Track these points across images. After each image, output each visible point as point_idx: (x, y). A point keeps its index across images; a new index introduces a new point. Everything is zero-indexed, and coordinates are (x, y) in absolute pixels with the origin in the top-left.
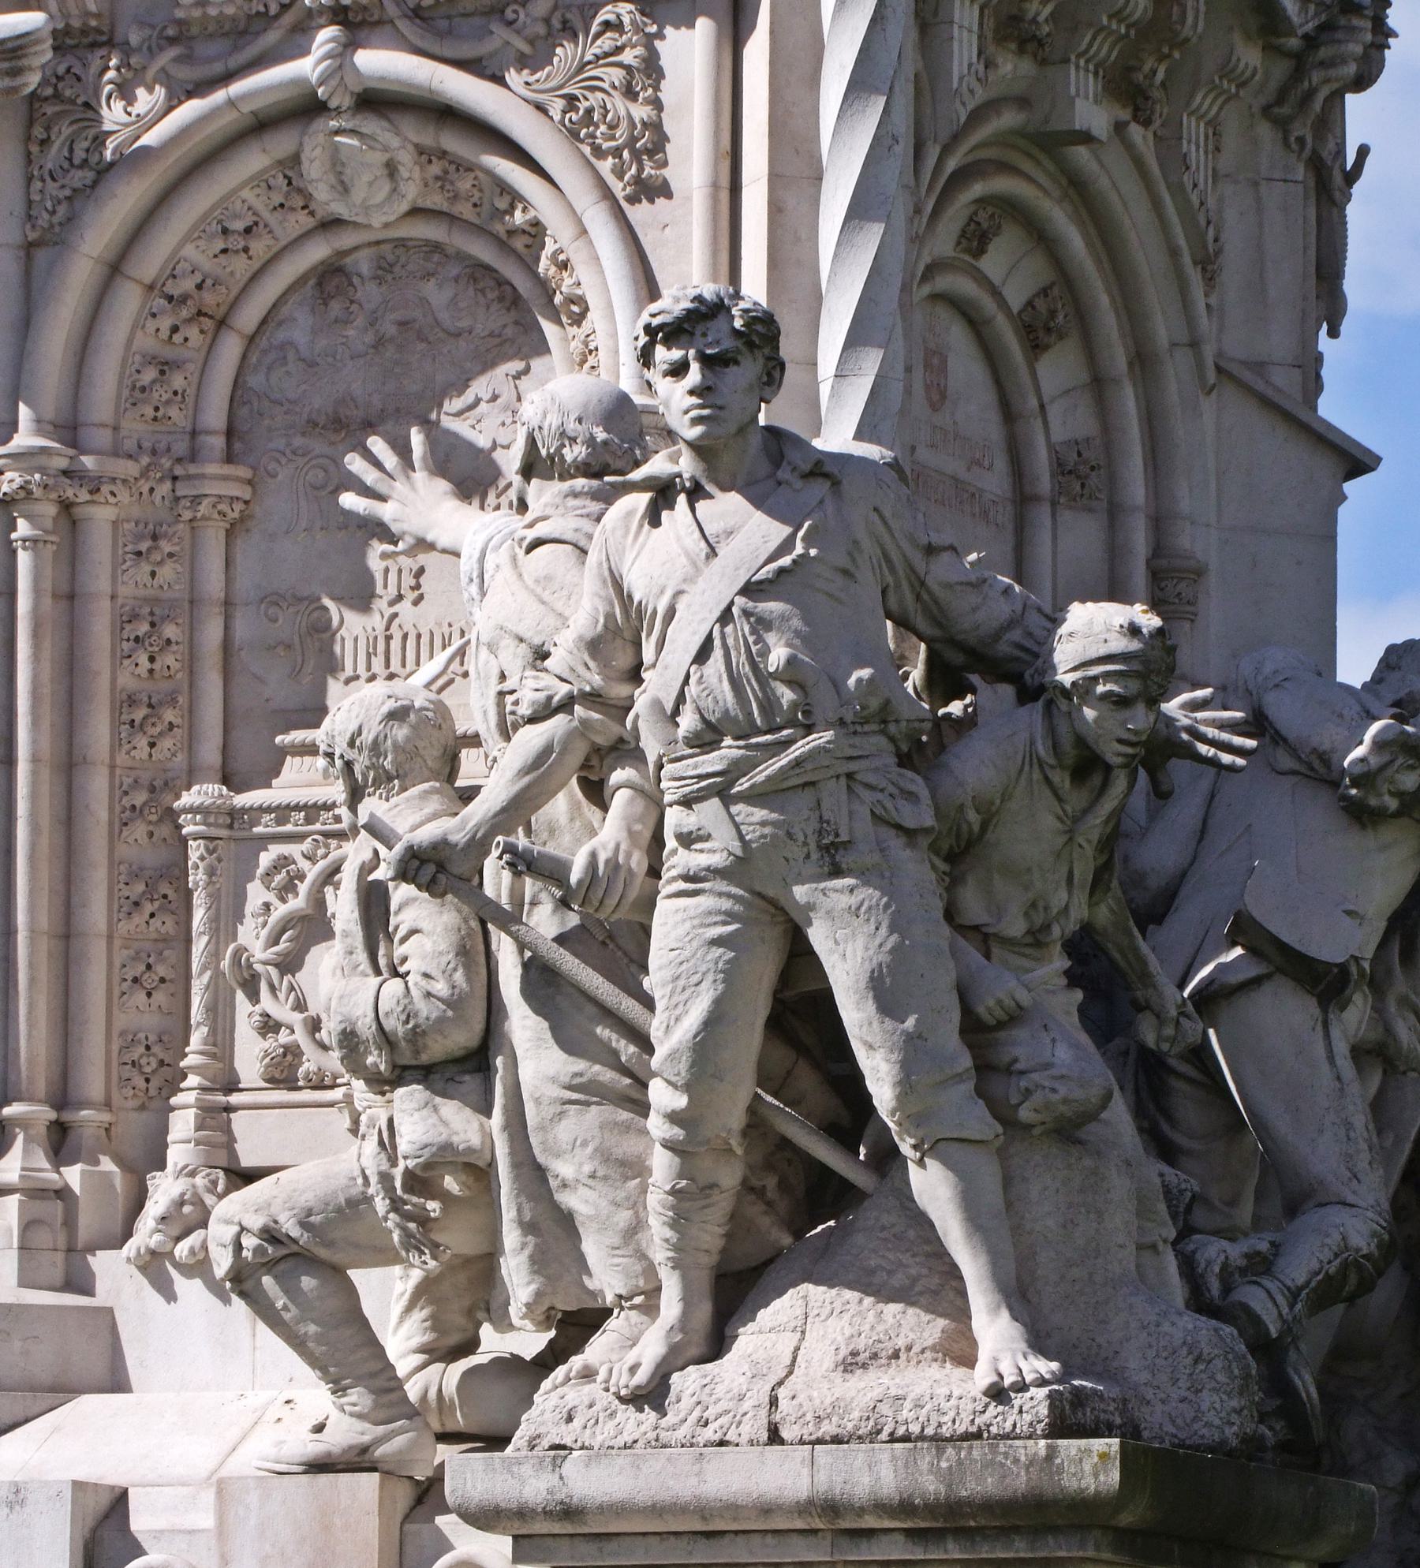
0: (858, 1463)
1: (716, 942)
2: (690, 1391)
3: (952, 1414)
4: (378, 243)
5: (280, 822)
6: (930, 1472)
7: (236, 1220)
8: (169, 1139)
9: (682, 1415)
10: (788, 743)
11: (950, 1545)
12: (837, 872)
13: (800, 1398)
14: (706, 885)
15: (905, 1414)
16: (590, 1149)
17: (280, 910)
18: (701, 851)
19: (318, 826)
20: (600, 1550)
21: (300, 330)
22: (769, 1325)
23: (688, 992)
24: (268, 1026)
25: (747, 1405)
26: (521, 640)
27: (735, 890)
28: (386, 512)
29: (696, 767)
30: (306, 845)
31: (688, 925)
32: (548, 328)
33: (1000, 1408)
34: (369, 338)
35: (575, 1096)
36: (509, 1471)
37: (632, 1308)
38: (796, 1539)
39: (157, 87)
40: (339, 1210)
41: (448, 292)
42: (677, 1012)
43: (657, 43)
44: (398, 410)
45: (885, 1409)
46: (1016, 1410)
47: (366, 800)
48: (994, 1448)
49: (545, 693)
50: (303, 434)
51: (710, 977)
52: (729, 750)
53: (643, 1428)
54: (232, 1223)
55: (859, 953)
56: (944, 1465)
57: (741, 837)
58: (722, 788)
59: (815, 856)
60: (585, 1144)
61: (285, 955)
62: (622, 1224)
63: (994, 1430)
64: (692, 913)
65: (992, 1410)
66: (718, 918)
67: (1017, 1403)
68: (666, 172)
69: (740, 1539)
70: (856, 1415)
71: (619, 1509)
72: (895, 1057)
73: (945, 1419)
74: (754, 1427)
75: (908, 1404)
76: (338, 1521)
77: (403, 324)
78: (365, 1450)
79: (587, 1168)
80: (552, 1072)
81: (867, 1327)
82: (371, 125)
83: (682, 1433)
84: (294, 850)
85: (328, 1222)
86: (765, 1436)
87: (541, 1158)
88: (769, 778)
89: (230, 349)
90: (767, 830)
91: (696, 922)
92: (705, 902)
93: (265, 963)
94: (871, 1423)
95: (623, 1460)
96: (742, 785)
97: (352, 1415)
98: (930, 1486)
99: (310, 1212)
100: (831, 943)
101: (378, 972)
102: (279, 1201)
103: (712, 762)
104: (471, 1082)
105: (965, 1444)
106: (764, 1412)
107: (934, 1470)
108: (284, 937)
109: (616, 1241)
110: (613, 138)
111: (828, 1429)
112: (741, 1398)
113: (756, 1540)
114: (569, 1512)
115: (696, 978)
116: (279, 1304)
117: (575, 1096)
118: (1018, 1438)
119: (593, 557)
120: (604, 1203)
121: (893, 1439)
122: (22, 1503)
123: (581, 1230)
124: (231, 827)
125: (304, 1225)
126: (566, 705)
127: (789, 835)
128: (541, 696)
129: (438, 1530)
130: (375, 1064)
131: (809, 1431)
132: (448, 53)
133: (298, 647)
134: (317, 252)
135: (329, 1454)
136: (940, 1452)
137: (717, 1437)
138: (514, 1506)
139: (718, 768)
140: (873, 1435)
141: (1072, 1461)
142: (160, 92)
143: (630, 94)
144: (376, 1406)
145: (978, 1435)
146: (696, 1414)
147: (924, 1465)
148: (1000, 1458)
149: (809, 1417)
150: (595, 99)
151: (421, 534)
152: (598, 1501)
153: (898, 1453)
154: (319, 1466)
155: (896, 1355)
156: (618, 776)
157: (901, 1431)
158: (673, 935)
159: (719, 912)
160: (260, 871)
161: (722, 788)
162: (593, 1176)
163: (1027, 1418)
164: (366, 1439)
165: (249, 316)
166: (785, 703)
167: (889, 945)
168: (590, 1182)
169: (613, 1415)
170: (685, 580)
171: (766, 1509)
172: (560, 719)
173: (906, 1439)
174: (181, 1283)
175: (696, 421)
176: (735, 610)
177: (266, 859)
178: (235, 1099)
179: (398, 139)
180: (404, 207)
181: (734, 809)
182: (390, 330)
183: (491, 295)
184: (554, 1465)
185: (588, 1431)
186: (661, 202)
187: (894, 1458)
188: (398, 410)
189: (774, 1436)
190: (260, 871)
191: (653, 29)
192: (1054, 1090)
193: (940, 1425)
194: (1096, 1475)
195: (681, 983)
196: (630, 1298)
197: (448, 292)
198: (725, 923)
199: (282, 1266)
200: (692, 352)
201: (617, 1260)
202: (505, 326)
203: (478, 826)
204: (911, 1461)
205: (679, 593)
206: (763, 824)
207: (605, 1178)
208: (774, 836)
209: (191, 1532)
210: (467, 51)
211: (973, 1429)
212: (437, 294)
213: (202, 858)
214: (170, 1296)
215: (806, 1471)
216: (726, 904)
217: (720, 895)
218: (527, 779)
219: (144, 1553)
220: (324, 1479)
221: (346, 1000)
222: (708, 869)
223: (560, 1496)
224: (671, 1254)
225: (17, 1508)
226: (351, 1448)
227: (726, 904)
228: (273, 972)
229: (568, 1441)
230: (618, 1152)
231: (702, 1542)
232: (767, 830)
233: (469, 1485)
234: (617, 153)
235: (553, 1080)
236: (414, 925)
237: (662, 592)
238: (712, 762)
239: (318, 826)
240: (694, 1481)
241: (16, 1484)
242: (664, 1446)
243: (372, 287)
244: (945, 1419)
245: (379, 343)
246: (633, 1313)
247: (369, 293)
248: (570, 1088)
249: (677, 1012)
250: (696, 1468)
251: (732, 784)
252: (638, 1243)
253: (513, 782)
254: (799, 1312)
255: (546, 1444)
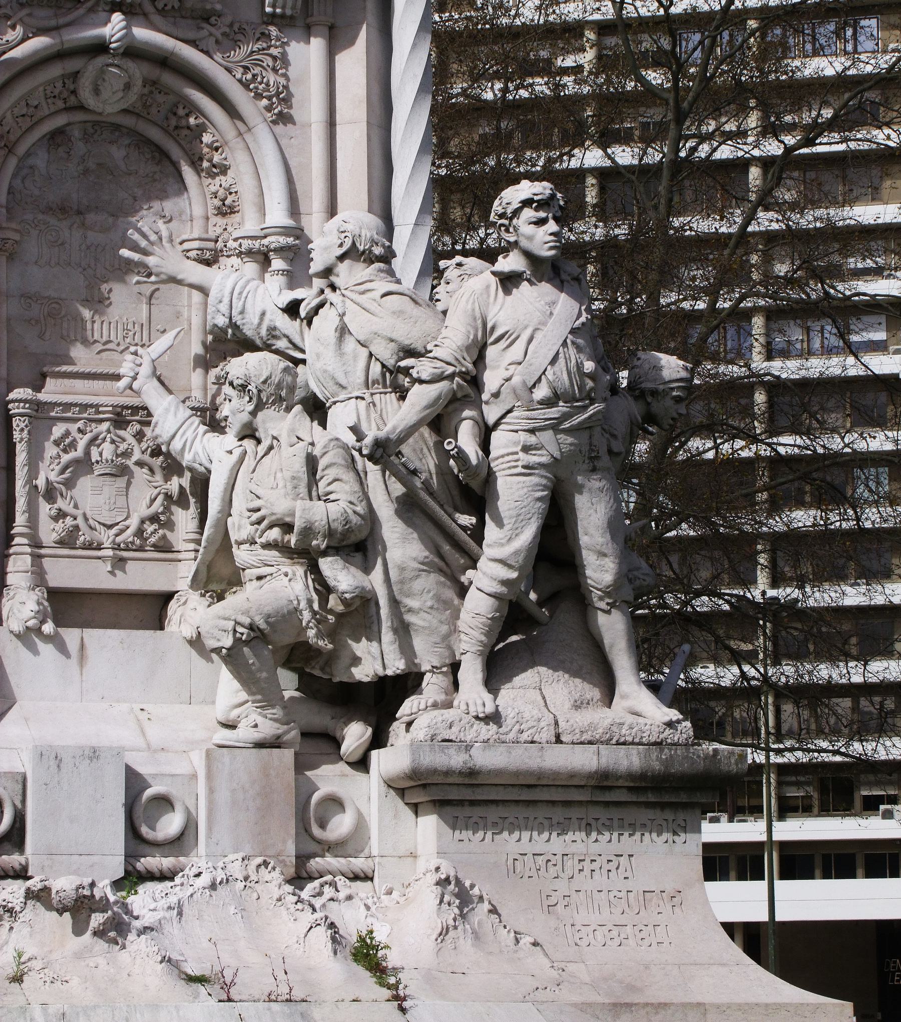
0: (621, 754)
1: (539, 499)
2: (511, 716)
3: (648, 733)
4: (85, 122)
5: (63, 411)
6: (657, 760)
7: (233, 618)
8: (8, 570)
9: (509, 728)
10: (585, 408)
11: (650, 795)
12: (594, 470)
13: (571, 722)
14: (537, 471)
15: (623, 732)
16: (431, 594)
17: (66, 458)
18: (534, 455)
19: (85, 415)
20: (473, 792)
21: (40, 160)
22: (519, 685)
23: (524, 523)
24: (61, 515)
25: (543, 724)
26: (392, 340)
27: (549, 475)
28: (151, 261)
29: (544, 414)
30: (80, 424)
31: (525, 490)
32: (187, 172)
33: (671, 731)
34: (81, 168)
35: (425, 568)
36: (443, 752)
37: (442, 673)
38: (573, 790)
39: (18, 27)
40: (283, 616)
41: (123, 152)
42: (517, 532)
43: (287, 48)
44: (97, 207)
45: (614, 729)
46: (679, 732)
47: (265, 411)
48: (688, 750)
49: (441, 370)
50: (43, 213)
51: (536, 516)
52: (563, 407)
53: (490, 733)
54: (230, 619)
55: (603, 510)
56: (664, 757)
57: (560, 450)
58: (555, 426)
59: (587, 461)
60: (429, 591)
61: (67, 479)
62: (443, 632)
63: (669, 741)
64: (528, 484)
65: (668, 732)
66: (541, 488)
67: (679, 728)
68: (292, 112)
69: (545, 789)
70: (601, 731)
71: (499, 772)
72: (617, 561)
73: (645, 735)
74: (547, 735)
75: (625, 727)
76: (272, 772)
77: (99, 165)
78: (279, 737)
79: (429, 604)
80: (414, 555)
81: (572, 688)
82: (130, 65)
83: (511, 736)
84: (73, 427)
85: (277, 622)
86: (554, 739)
87: (398, 597)
88: (579, 423)
89: (12, 162)
90: (572, 448)
91: (530, 489)
92: (534, 480)
93: (58, 483)
94: (608, 735)
95: (502, 748)
96: (566, 425)
97: (271, 719)
98: (657, 766)
99: (269, 616)
100: (590, 504)
101: (311, 499)
102: (254, 609)
103: (554, 412)
104: (358, 557)
105: (674, 747)
106: (552, 728)
107: (658, 759)
108: (68, 471)
109: (438, 640)
110: (268, 91)
111: (586, 737)
112: (539, 720)
113: (553, 789)
114: (472, 773)
115: (529, 516)
116: (251, 661)
117: (425, 568)
118: (680, 745)
119: (322, 297)
120: (435, 621)
121: (618, 743)
122: (98, 758)
123: (412, 633)
124: (37, 411)
125: (267, 622)
126: (451, 377)
127: (580, 451)
128: (438, 371)
129: (309, 779)
130: (318, 545)
131: (576, 738)
132: (181, 36)
133: (43, 322)
134: (60, 121)
135: (265, 738)
136: (662, 751)
137: (530, 739)
138: (445, 769)
139: (556, 416)
140: (608, 742)
141: (725, 757)
142: (19, 30)
143: (275, 70)
144: (286, 715)
145: (660, 743)
146: (517, 727)
147: (654, 756)
148: (691, 755)
149: (577, 731)
150: (257, 70)
151: (174, 275)
152: (490, 767)
153: (641, 751)
154: (260, 745)
155: (588, 703)
156: (467, 413)
157: (622, 740)
158: (517, 494)
159: (541, 485)
160: (52, 438)
161: (555, 426)
162: (431, 608)
163: (685, 736)
164: (280, 731)
165: (21, 149)
166: (588, 387)
167: (614, 507)
168: (429, 610)
169: (472, 726)
170: (539, 324)
171: (448, 773)
172: (443, 385)
173: (624, 744)
174: (41, 645)
175: (551, 248)
176: (568, 341)
177: (58, 430)
178: (43, 551)
179: (138, 71)
180: (124, 105)
181: (559, 436)
182: (91, 165)
183: (147, 156)
184: (466, 750)
185: (462, 734)
186: (290, 126)
187: (639, 753)
188: (97, 207)
189: (558, 740)
190: (52, 438)
191: (285, 40)
192: (644, 580)
193: (642, 738)
194: (737, 765)
195: (521, 518)
196: (441, 668)
197: (123, 152)
198: (543, 491)
199: (253, 643)
200: (550, 215)
201: (436, 649)
202: (155, 173)
203: (401, 432)
204: (647, 755)
205: (536, 330)
206: (571, 444)
207: (437, 609)
208: (574, 451)
209: (173, 775)
210: (191, 35)
211: (659, 740)
212: (118, 153)
213: (26, 426)
214: (35, 652)
215: (595, 758)
216: (544, 482)
217: (542, 476)
218: (428, 411)
219: (151, 787)
220: (265, 751)
221: (307, 512)
222: (539, 464)
223: (470, 765)
224: (481, 648)
225: (95, 760)
226: (274, 735)
227: (544, 482)
228: (63, 488)
229: (453, 737)
230: (444, 597)
231: (526, 790)
232: (572, 448)
233: (422, 758)
234: (269, 98)
235: (415, 559)
236: (337, 477)
237: (526, 328)
238: (554, 412)
239: (85, 415)
240: (539, 760)
241: (93, 748)
242: (503, 742)
243: (81, 144)
244: (645, 735)
245: (86, 172)
246: (440, 676)
247: (80, 148)
248: (422, 563)
249: (517, 532)
250: (540, 754)
251: (561, 423)
252: (449, 642)
253: (421, 411)
254: (537, 679)
255: (439, 738)
